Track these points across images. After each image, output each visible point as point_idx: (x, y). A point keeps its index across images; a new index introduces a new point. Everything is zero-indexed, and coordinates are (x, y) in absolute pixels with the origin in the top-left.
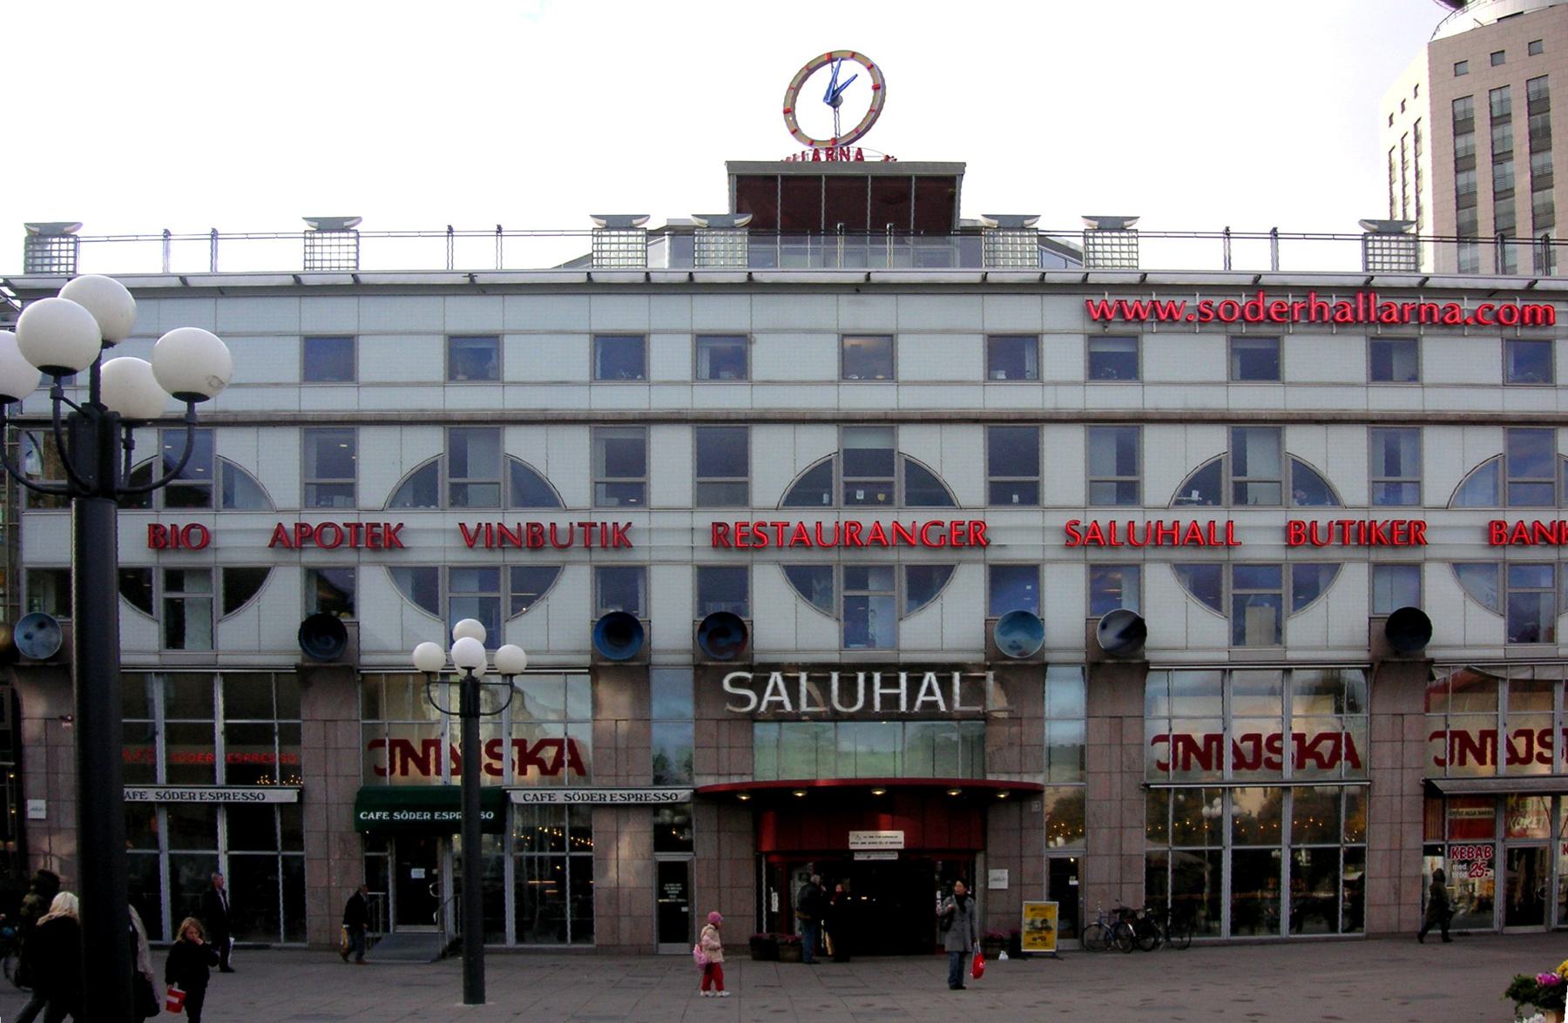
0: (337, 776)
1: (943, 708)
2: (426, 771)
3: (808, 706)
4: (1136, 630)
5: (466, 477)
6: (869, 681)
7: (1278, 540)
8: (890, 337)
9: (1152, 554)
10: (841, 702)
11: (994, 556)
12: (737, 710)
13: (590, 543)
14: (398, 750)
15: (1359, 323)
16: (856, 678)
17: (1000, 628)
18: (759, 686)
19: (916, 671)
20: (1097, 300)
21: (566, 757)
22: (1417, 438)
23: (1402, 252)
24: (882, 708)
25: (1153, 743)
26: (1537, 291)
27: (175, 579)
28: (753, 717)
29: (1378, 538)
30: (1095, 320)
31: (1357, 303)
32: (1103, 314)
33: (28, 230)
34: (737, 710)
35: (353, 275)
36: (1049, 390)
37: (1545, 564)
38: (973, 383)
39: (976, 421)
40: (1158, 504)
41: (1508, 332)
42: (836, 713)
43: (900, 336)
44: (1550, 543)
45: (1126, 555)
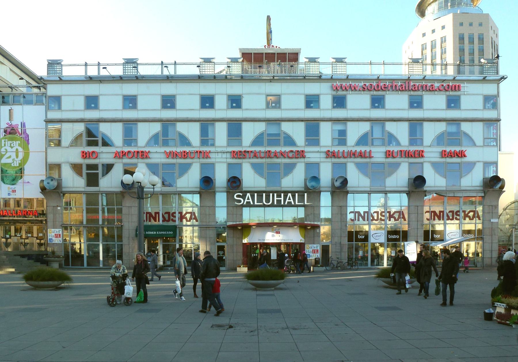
0: (132, 222)
1: (293, 203)
2: (155, 221)
3: (298, 203)
4: (345, 182)
5: (168, 137)
6: (273, 196)
7: (383, 155)
8: (279, 96)
9: (349, 160)
10: (266, 202)
11: (306, 160)
12: (238, 204)
13: (199, 157)
14: (357, 214)
15: (406, 90)
16: (270, 195)
17: (309, 180)
18: (244, 197)
19: (286, 193)
20: (335, 84)
21: (476, 215)
22: (213, 125)
23: (204, 70)
24: (277, 203)
25: (425, 213)
26: (487, 80)
27: (90, 167)
28: (243, 206)
29: (411, 155)
30: (334, 90)
31: (406, 84)
32: (337, 88)
33: (48, 62)
34: (238, 204)
35: (59, 77)
36: (322, 112)
37: (420, 163)
38: (196, 110)
39: (302, 121)
40: (246, 145)
41: (448, 93)
42: (264, 205)
43: (321, 95)
44: (459, 157)
45: (342, 160)
